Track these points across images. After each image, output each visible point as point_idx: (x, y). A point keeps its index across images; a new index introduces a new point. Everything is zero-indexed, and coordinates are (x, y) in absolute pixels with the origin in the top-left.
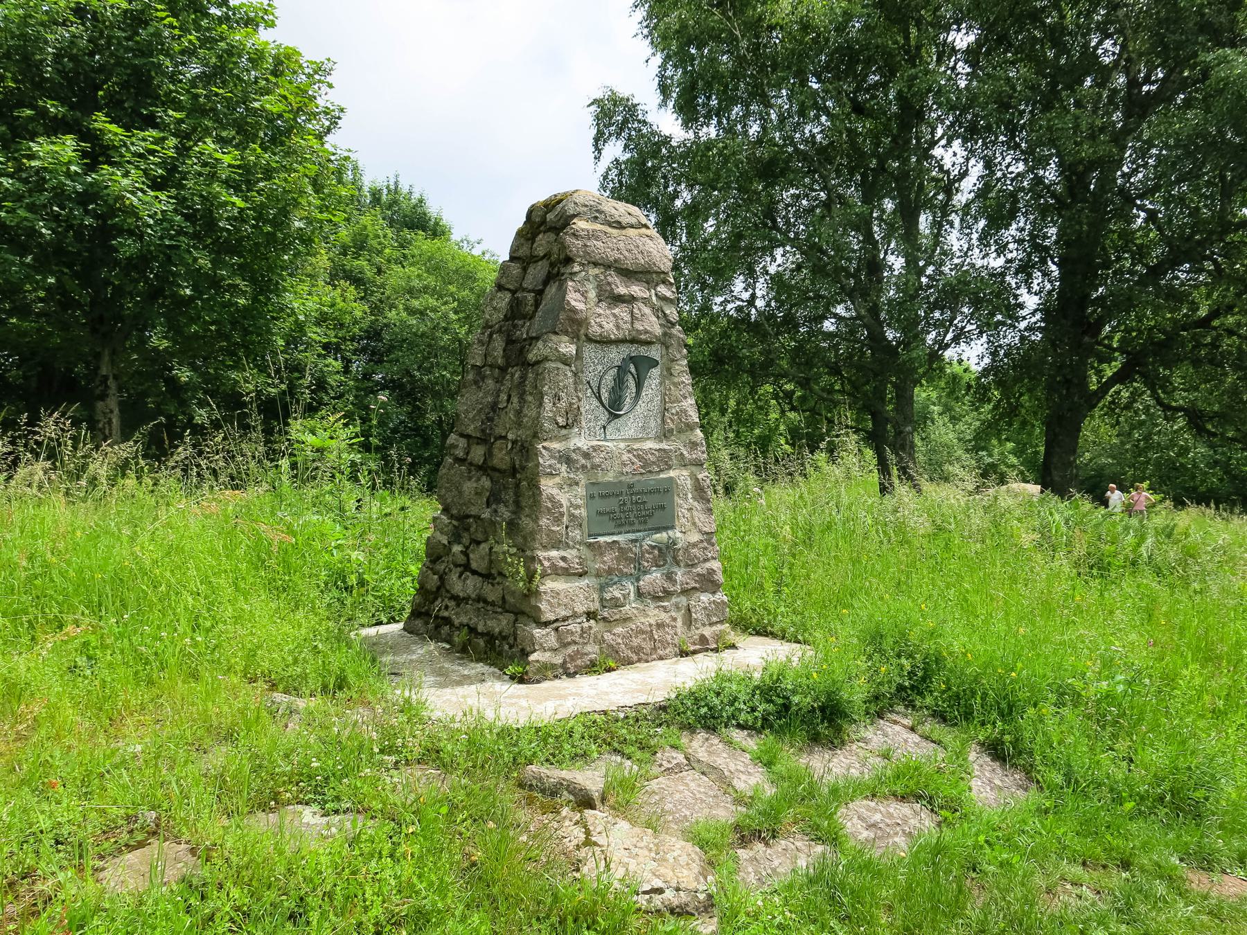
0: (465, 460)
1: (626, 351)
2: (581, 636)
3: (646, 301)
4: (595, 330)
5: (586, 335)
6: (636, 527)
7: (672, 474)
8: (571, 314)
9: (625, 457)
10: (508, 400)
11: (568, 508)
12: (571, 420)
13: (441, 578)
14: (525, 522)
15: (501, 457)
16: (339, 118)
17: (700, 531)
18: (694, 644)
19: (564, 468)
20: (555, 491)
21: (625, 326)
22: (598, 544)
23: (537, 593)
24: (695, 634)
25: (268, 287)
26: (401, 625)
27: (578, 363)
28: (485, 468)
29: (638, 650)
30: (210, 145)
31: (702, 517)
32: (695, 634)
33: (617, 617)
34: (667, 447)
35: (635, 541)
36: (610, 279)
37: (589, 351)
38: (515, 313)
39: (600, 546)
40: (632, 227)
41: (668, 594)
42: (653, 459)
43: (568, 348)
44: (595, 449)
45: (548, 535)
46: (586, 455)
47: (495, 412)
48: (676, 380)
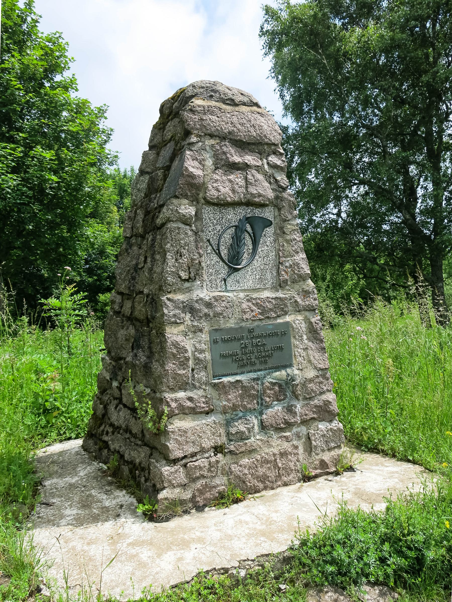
0: (120, 312)
1: (242, 212)
2: (209, 470)
3: (258, 169)
4: (212, 193)
5: (205, 199)
6: (258, 367)
7: (288, 319)
8: (190, 179)
9: (244, 306)
10: (145, 262)
11: (193, 353)
12: (194, 274)
13: (105, 408)
14: (155, 366)
15: (141, 310)
16: (111, 135)
17: (316, 368)
18: (316, 469)
19: (188, 316)
20: (179, 339)
21: (240, 190)
22: (223, 385)
23: (166, 433)
24: (316, 459)
25: (75, 224)
26: (80, 442)
27: (198, 224)
28: (131, 319)
29: (263, 479)
30: (39, 149)
31: (317, 355)
32: (316, 459)
33: (243, 449)
34: (282, 296)
35: (258, 379)
36: (225, 149)
37: (208, 213)
38: (153, 189)
39: (224, 386)
40: (244, 104)
41: (289, 425)
42: (269, 306)
43: (187, 209)
44: (216, 299)
45: (174, 378)
46: (209, 305)
47: (136, 272)
48: (288, 237)
